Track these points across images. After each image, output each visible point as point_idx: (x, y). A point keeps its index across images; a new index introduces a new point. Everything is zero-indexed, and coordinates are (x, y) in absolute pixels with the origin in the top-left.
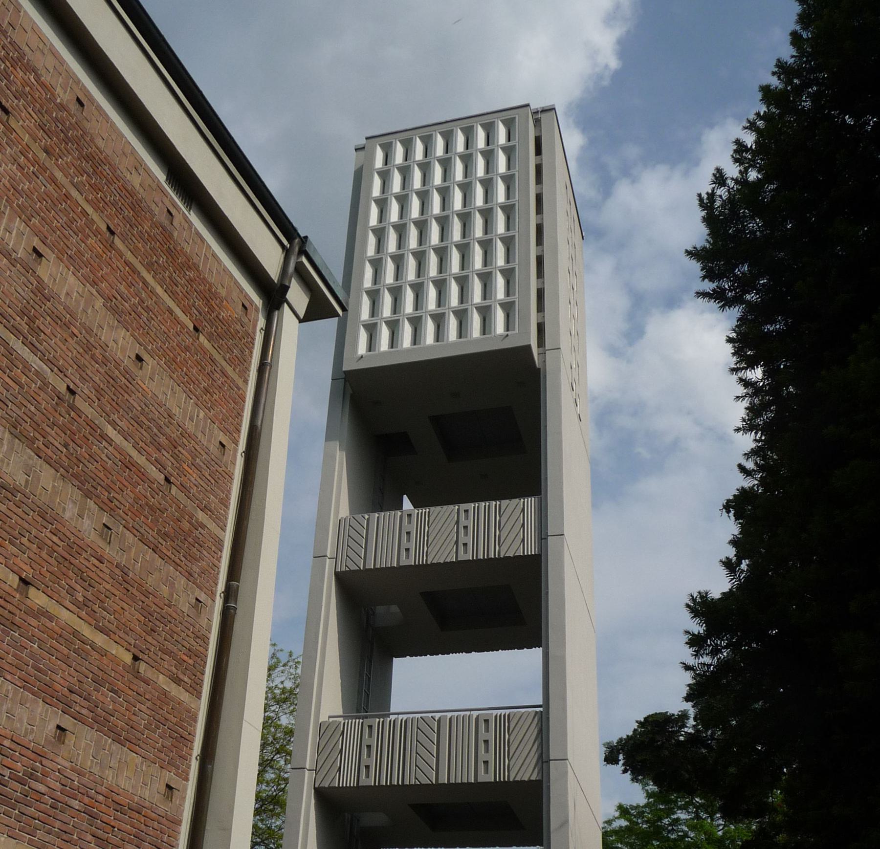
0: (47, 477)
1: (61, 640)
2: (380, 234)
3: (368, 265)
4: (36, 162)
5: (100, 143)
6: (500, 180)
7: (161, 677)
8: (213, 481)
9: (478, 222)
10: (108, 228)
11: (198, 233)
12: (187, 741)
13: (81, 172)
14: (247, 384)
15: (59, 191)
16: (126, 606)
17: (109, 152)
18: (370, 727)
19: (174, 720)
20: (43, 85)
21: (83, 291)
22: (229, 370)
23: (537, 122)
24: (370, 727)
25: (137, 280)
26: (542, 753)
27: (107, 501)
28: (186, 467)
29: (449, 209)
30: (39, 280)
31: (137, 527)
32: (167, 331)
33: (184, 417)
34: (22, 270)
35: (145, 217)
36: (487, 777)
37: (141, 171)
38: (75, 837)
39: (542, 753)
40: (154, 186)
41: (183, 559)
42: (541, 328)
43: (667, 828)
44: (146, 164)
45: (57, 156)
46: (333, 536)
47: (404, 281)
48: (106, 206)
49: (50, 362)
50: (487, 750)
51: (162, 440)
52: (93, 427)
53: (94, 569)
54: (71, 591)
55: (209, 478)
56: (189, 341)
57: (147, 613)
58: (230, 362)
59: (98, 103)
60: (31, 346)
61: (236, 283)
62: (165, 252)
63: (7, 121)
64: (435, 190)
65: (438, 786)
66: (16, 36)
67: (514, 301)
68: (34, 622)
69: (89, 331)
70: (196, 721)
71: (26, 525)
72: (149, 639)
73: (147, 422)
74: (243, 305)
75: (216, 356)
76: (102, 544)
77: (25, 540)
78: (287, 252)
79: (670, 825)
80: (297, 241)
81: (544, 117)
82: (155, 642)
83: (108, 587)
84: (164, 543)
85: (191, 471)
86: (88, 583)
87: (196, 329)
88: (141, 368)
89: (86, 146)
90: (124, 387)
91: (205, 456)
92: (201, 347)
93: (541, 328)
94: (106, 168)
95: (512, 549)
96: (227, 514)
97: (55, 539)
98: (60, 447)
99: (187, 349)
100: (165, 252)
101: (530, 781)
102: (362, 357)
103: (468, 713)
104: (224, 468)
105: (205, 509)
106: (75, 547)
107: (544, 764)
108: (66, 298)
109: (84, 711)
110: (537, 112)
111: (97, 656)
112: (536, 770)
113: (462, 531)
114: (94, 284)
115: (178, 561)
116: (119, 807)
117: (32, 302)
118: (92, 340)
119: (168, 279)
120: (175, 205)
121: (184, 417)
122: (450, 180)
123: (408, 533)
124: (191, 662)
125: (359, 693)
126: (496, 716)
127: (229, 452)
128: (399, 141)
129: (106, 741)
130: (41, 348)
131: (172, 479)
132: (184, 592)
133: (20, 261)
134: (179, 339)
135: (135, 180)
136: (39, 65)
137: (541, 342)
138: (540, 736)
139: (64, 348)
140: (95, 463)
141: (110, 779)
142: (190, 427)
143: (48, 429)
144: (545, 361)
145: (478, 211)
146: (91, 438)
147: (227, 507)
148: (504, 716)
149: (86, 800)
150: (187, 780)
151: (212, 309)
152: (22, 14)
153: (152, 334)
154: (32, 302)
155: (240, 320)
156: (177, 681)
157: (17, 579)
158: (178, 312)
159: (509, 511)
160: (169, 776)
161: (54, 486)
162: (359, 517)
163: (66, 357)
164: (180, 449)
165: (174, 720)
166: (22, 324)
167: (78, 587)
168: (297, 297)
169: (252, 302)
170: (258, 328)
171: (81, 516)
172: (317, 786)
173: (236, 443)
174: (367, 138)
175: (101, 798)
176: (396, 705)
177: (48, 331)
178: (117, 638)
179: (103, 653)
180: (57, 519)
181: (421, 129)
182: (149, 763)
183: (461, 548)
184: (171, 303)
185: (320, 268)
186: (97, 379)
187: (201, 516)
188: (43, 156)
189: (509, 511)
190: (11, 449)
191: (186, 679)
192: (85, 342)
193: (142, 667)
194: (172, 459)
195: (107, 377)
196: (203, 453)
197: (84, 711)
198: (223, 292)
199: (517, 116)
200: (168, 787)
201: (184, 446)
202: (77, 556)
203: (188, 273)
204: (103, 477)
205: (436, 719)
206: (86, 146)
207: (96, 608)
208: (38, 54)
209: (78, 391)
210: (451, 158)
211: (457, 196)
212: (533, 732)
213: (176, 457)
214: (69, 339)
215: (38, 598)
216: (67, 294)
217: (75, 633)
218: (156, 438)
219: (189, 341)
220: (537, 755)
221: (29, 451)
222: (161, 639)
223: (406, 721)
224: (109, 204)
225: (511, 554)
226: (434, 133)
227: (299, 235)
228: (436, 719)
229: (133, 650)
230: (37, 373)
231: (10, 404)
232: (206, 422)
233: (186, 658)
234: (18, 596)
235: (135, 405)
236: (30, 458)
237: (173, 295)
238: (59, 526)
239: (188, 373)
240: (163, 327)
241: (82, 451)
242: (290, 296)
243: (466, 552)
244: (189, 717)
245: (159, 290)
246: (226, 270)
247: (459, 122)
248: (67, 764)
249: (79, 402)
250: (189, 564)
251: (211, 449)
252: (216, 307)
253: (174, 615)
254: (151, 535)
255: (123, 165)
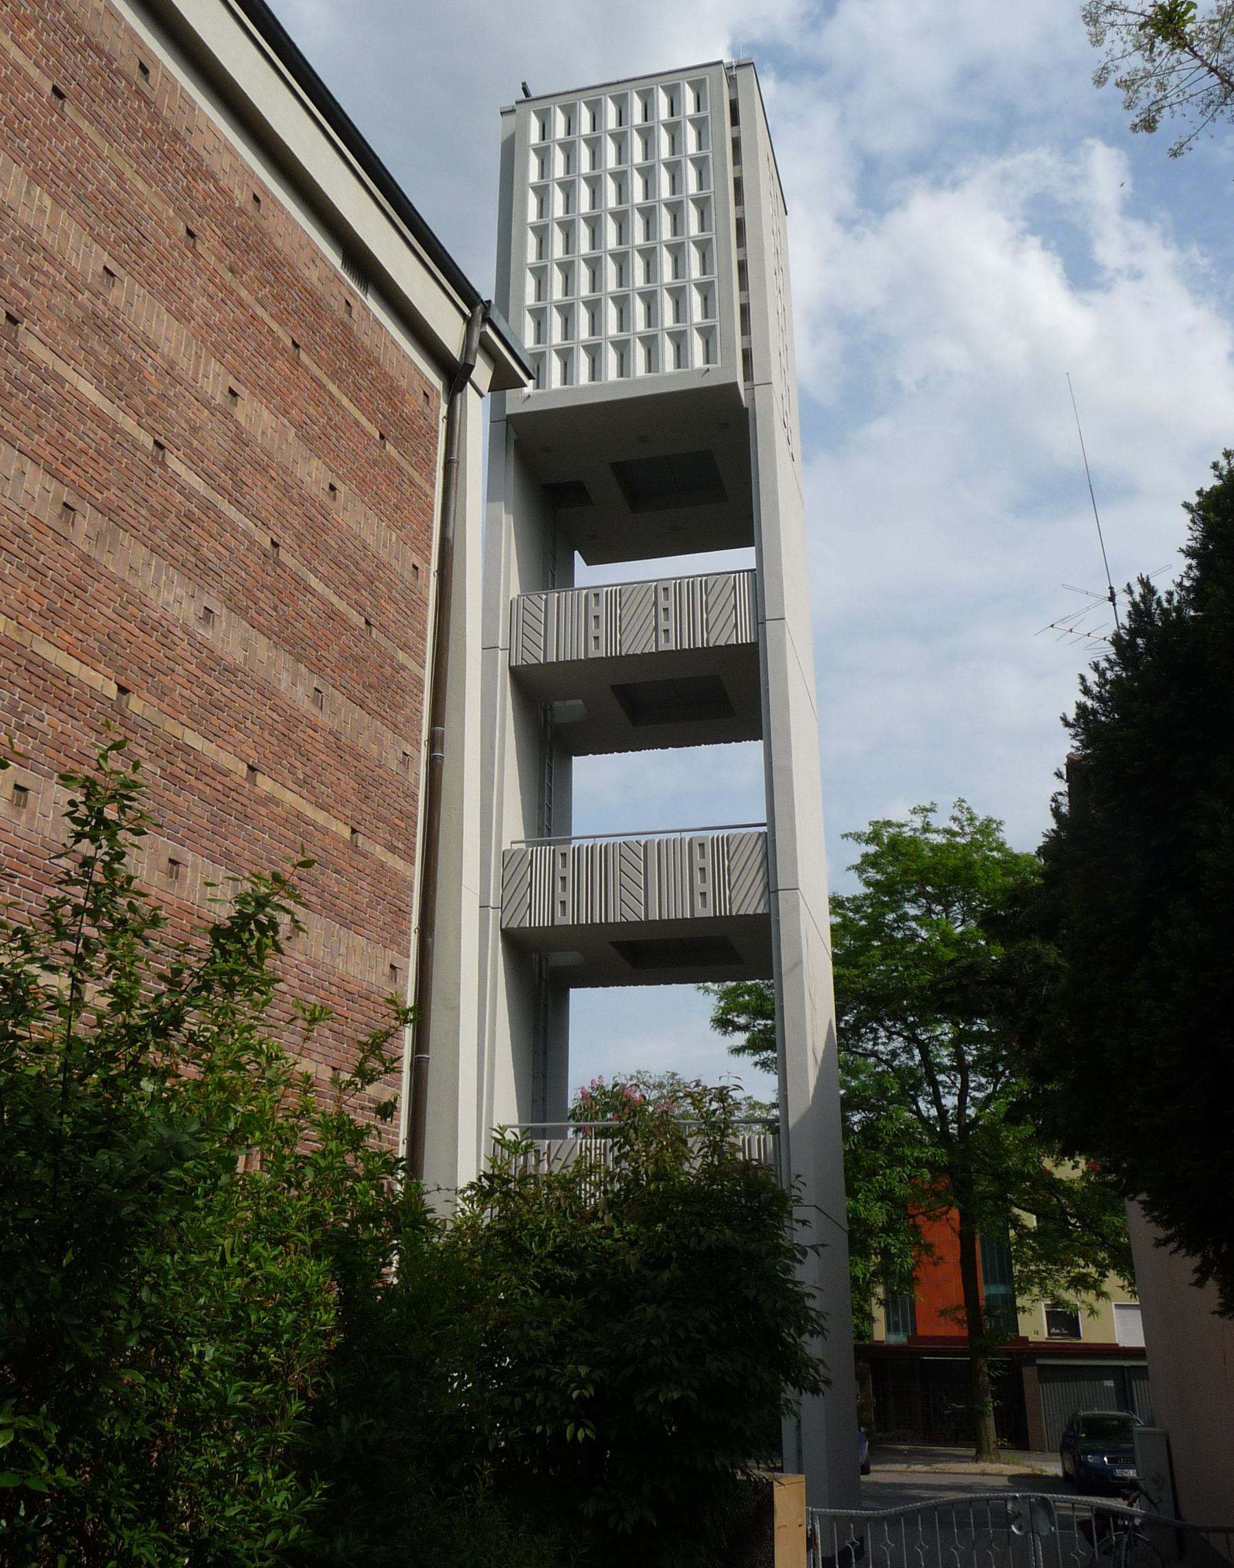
0: (262, 645)
1: (288, 826)
2: (542, 233)
3: (529, 274)
4: (223, 287)
5: (278, 242)
6: (689, 164)
7: (378, 847)
8: (409, 613)
9: (665, 219)
10: (294, 342)
11: (376, 320)
12: (403, 913)
13: (264, 283)
14: (434, 488)
15: (245, 312)
16: (341, 776)
17: (286, 250)
18: (564, 855)
19: (392, 892)
20: (220, 190)
21: (277, 426)
22: (416, 475)
23: (732, 80)
24: (564, 855)
25: (324, 395)
26: (768, 883)
27: (316, 662)
28: (383, 603)
29: (627, 202)
30: (238, 425)
31: (344, 683)
32: (355, 448)
33: (378, 546)
34: (222, 418)
35: (326, 318)
36: (705, 911)
37: (318, 262)
38: (315, 1034)
39: (768, 883)
40: (331, 276)
41: (388, 710)
42: (747, 355)
43: (891, 926)
44: (322, 252)
45: (241, 272)
46: (504, 623)
47: (576, 297)
48: (290, 317)
49: (254, 517)
50: (704, 880)
51: (361, 578)
52: (297, 580)
53: (310, 740)
54: (292, 770)
55: (406, 610)
56: (375, 452)
57: (361, 780)
58: (415, 466)
59: (272, 194)
60: (237, 504)
61: (416, 368)
62: (347, 353)
63: (194, 247)
64: (608, 176)
65: (648, 923)
66: (195, 142)
67: (715, 326)
68: (263, 811)
69: (285, 470)
70: (412, 891)
71: (249, 707)
72: (364, 807)
73: (344, 561)
74: (425, 394)
75: (404, 464)
76: (315, 710)
77: (248, 723)
78: (469, 322)
79: (895, 921)
80: (479, 308)
81: (740, 74)
82: (369, 810)
83: (324, 757)
84: (369, 696)
85: (388, 607)
86: (306, 757)
87: (382, 437)
88: (334, 499)
89: (266, 249)
90: (321, 526)
91: (401, 585)
92: (389, 457)
93: (747, 355)
94: (286, 270)
95: (723, 636)
96: (425, 647)
97: (274, 716)
98: (271, 611)
99: (375, 463)
100: (347, 353)
101: (755, 915)
102: (529, 396)
103: (677, 835)
104: (419, 595)
105: (404, 647)
106: (293, 720)
107: (772, 895)
108: (262, 439)
109: (314, 899)
110: (732, 67)
111: (320, 836)
112: (763, 901)
113: (661, 614)
114: (285, 413)
115: (384, 714)
116: (350, 996)
117: (233, 453)
118: (288, 480)
119: (352, 385)
120: (352, 293)
121: (378, 546)
122: (627, 162)
123: (596, 617)
124: (403, 825)
125: (541, 807)
126: (713, 839)
127: (422, 574)
128: (559, 107)
129: (334, 927)
130: (245, 502)
131: (372, 621)
132: (391, 747)
133: (218, 407)
134: (367, 453)
135: (312, 275)
136: (216, 169)
137: (748, 375)
138: (765, 864)
139: (265, 496)
140: (302, 621)
141: (341, 967)
142: (384, 555)
143: (259, 594)
144: (753, 399)
145: (665, 204)
146: (296, 593)
147: (424, 639)
148: (723, 838)
149: (322, 993)
150: (408, 957)
151: (395, 408)
152: (196, 112)
153: (342, 455)
154: (233, 453)
155: (423, 413)
156: (392, 849)
157: (246, 766)
158: (364, 421)
159: (718, 588)
160: (392, 955)
161: (268, 657)
162: (535, 598)
163: (267, 507)
164: (377, 583)
165: (392, 892)
166: (225, 479)
167: (298, 765)
168: (482, 373)
169: (432, 387)
170: (441, 417)
171: (294, 684)
172: (503, 927)
173: (428, 562)
174: (517, 103)
175: (334, 989)
176: (1142, 1345)
177: (249, 482)
178: (337, 814)
179: (325, 832)
180: (275, 693)
181: (586, 92)
182: (373, 944)
183: (662, 635)
184: (357, 414)
185: (505, 336)
186: (296, 524)
187: (401, 656)
188: (228, 276)
189: (718, 588)
190: (229, 625)
191: (400, 846)
192: (283, 483)
193: (361, 839)
194: (370, 597)
195: (305, 519)
196: (397, 582)
197: (314, 899)
198: (404, 383)
199: (708, 77)
200: (393, 967)
201: (380, 579)
202: (294, 729)
203: (369, 371)
204: (311, 635)
205: (642, 844)
206: (266, 249)
207: (315, 783)
208: (215, 154)
209: (281, 542)
210: (626, 132)
211: (637, 184)
212: (757, 857)
213: (373, 594)
214: (269, 486)
215: (265, 784)
216: (263, 433)
217: (299, 815)
218: (354, 577)
219: (375, 452)
220: (762, 885)
221: (244, 623)
222: (375, 806)
223: (606, 847)
224: (292, 313)
225: (721, 642)
226: (603, 97)
227: (482, 301)
228: (642, 844)
229: (351, 823)
230: (245, 534)
231: (223, 574)
232: (398, 545)
233: (398, 822)
234: (247, 786)
235: (333, 544)
236: (247, 631)
237: (355, 400)
238: (277, 701)
239: (379, 492)
240: (351, 444)
241: (290, 611)
242: (474, 376)
243: (667, 640)
244: (407, 887)
245: (345, 401)
246: (406, 356)
247: (634, 83)
248: (303, 958)
249: (284, 556)
250: (394, 714)
251: (405, 575)
252: (399, 404)
253: (385, 776)
254: (358, 690)
255: (300, 259)
